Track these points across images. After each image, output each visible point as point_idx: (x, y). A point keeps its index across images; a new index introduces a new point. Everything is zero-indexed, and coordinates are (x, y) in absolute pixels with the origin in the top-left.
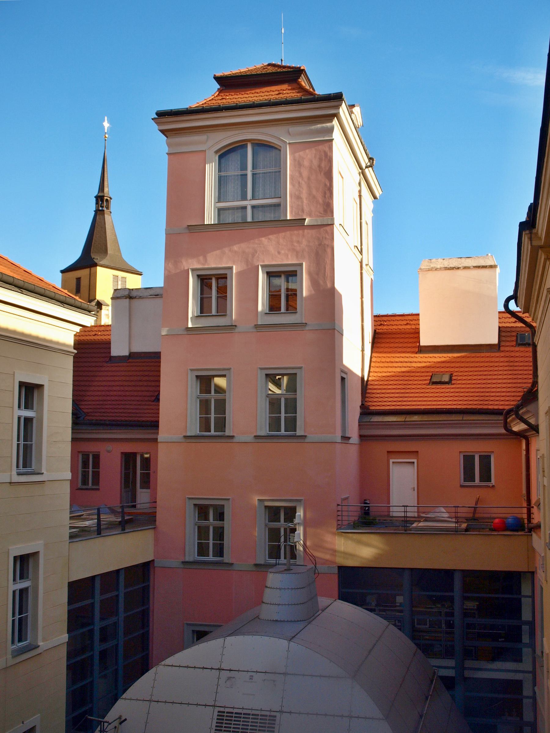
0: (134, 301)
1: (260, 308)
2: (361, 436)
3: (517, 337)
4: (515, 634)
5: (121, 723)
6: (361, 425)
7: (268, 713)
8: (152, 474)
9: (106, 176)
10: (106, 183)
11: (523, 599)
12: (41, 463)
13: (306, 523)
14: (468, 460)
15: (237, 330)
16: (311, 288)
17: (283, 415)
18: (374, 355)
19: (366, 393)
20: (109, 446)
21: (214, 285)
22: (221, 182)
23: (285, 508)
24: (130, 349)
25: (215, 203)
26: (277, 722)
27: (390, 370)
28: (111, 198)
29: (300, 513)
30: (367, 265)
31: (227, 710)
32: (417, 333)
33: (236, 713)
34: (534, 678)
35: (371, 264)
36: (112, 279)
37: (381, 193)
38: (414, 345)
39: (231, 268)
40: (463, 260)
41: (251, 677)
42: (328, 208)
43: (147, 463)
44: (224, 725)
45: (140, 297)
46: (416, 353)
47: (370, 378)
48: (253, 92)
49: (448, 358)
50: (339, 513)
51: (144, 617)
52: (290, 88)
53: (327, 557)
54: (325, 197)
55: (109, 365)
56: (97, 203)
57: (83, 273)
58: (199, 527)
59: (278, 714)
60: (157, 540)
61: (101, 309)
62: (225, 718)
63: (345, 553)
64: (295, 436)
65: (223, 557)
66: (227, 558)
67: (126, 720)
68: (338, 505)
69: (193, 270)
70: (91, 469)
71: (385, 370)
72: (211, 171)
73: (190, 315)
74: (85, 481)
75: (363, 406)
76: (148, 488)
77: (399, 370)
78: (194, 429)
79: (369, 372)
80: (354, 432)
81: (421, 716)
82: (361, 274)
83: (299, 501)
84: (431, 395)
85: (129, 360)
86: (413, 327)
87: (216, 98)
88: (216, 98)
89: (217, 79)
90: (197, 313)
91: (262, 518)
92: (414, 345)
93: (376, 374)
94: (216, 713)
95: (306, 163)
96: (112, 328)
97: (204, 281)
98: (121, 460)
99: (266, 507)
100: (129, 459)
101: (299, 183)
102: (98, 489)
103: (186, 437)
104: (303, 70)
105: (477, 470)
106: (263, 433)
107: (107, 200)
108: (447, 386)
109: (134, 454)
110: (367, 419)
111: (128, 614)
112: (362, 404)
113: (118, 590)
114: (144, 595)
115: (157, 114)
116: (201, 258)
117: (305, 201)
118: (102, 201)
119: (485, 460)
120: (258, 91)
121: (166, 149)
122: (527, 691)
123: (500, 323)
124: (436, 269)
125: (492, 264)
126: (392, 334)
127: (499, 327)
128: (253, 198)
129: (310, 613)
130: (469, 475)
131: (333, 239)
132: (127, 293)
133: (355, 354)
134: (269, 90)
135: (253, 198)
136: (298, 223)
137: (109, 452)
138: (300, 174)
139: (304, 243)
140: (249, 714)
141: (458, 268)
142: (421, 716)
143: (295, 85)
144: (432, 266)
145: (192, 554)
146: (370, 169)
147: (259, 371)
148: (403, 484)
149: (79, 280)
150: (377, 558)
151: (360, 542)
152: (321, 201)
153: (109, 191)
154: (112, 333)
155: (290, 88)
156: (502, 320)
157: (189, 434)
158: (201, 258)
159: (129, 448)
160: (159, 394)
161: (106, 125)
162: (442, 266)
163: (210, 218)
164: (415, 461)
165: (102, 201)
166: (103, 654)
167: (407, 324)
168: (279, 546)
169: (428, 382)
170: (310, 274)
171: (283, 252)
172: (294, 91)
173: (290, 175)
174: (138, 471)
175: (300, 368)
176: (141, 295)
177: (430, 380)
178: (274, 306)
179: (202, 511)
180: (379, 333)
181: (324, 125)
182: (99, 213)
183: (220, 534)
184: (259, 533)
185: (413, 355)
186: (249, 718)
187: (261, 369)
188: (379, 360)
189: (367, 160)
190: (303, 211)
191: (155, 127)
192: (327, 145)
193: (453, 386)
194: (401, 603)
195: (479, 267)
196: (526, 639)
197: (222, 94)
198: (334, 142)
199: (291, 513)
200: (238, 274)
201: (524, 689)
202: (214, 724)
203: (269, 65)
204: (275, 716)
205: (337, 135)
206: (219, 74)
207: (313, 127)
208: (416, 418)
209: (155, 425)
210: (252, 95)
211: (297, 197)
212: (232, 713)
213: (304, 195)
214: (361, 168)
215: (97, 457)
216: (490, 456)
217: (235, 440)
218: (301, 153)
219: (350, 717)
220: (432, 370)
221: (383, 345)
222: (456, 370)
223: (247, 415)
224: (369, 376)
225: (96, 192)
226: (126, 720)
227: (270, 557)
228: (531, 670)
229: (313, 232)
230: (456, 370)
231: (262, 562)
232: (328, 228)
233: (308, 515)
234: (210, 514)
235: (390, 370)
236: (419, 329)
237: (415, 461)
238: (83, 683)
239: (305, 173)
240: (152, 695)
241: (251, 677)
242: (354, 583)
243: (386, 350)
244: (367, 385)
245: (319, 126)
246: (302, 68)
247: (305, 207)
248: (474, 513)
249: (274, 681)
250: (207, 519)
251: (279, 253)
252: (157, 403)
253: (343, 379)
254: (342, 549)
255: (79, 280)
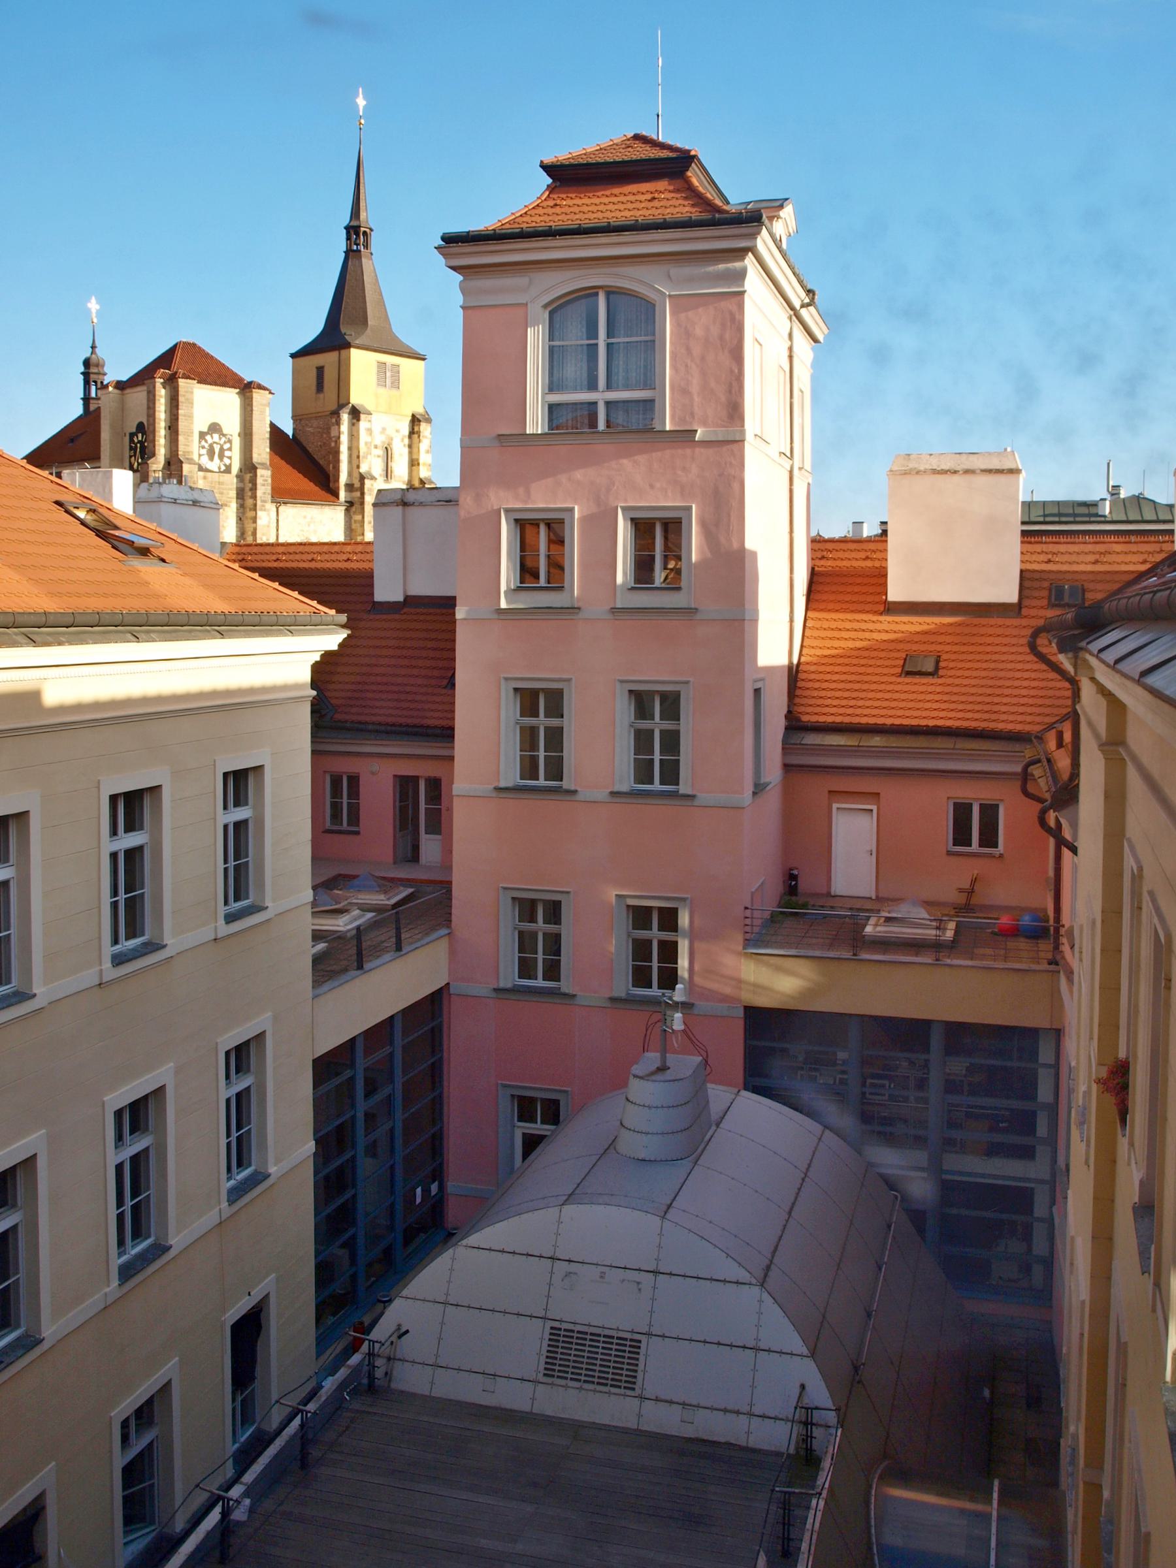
0: (410, 510)
1: (620, 579)
2: (787, 767)
3: (1050, 590)
4: (1026, 1121)
5: (400, 1337)
6: (786, 748)
7: (628, 1336)
8: (443, 811)
9: (362, 191)
10: (362, 204)
11: (1035, 1224)
12: (263, 892)
13: (693, 936)
14: (962, 812)
15: (581, 615)
16: (706, 549)
17: (657, 757)
18: (810, 614)
19: (795, 687)
20: (375, 765)
21: (542, 547)
22: (554, 356)
23: (660, 909)
24: (405, 591)
25: (544, 394)
26: (643, 1351)
27: (836, 644)
28: (371, 230)
29: (684, 920)
30: (800, 469)
31: (564, 1326)
32: (881, 576)
33: (579, 1332)
34: (1053, 1191)
35: (808, 466)
36: (374, 370)
37: (826, 331)
38: (877, 599)
39: (572, 510)
40: (964, 457)
41: (602, 1275)
42: (734, 411)
43: (436, 787)
44: (560, 1350)
45: (421, 504)
46: (881, 614)
47: (803, 659)
48: (608, 192)
49: (933, 626)
50: (748, 921)
51: (436, 1073)
52: (671, 188)
53: (728, 990)
54: (730, 392)
55: (372, 617)
56: (348, 238)
57: (328, 359)
58: (521, 933)
59: (643, 1338)
60: (452, 952)
61: (358, 420)
62: (561, 1339)
63: (755, 985)
64: (674, 795)
65: (559, 980)
66: (565, 985)
67: (407, 1332)
68: (746, 908)
69: (507, 511)
70: (345, 800)
71: (829, 643)
72: (536, 339)
73: (503, 587)
74: (336, 815)
75: (790, 716)
76: (439, 832)
77: (851, 644)
78: (511, 775)
79: (802, 646)
80: (773, 773)
81: (869, 1315)
82: (791, 491)
83: (684, 900)
84: (903, 696)
85: (405, 610)
86: (877, 564)
87: (545, 204)
88: (545, 204)
89: (548, 168)
90: (515, 583)
91: (623, 922)
92: (877, 599)
93: (812, 652)
94: (548, 1330)
95: (699, 331)
96: (375, 548)
97: (524, 526)
98: (394, 786)
99: (628, 906)
100: (406, 786)
101: (687, 366)
102: (358, 833)
103: (498, 789)
104: (695, 157)
105: (972, 827)
106: (624, 788)
107: (365, 233)
108: (930, 680)
109: (415, 779)
110: (797, 738)
111: (411, 1038)
112: (789, 712)
113: (391, 1043)
114: (434, 1039)
115: (443, 239)
116: (521, 490)
117: (696, 399)
118: (358, 235)
119: (990, 813)
120: (616, 191)
121: (459, 299)
122: (1039, 1211)
123: (1022, 562)
124: (918, 473)
125: (1013, 466)
126: (843, 575)
127: (1022, 571)
128: (609, 387)
129: (694, 1133)
130: (961, 836)
131: (743, 466)
132: (398, 496)
133: (777, 635)
134: (635, 191)
135: (609, 387)
136: (684, 436)
137: (373, 773)
138: (689, 350)
139: (695, 470)
140: (599, 1335)
141: (955, 472)
142: (869, 1315)
143: (679, 183)
144: (911, 465)
145: (509, 976)
146: (811, 308)
147: (618, 684)
148: (853, 848)
149: (320, 370)
150: (806, 994)
151: (778, 969)
152: (723, 399)
153: (368, 217)
154: (375, 555)
155: (671, 188)
156: (1026, 558)
157: (502, 784)
158: (521, 490)
159: (408, 769)
160: (454, 674)
161: (361, 102)
162: (928, 467)
163: (535, 422)
164: (874, 808)
165: (355, 233)
166: (370, 1117)
167: (867, 558)
168: (653, 962)
169: (899, 670)
170: (703, 524)
171: (658, 485)
172: (679, 196)
173: (672, 352)
174: (422, 806)
175: (687, 682)
176: (422, 500)
177: (903, 666)
178: (643, 568)
179: (527, 908)
180: (821, 574)
181: (730, 265)
182: (352, 255)
183: (554, 944)
184: (616, 946)
185: (875, 618)
186: (598, 1341)
187: (622, 682)
188: (818, 624)
189: (803, 294)
190: (692, 415)
191: (441, 260)
192: (735, 300)
193: (940, 681)
194: (844, 1061)
195: (990, 471)
196: (1042, 1130)
197: (555, 196)
198: (746, 296)
199: (669, 919)
200: (583, 519)
201: (1041, 1054)
202: (545, 1348)
203: (637, 137)
204: (640, 1341)
205: (754, 284)
206: (549, 159)
207: (711, 269)
208: (876, 741)
209: (447, 734)
210: (606, 200)
211: (682, 390)
212: (573, 1331)
213: (695, 388)
214: (792, 308)
215: (354, 780)
216: (997, 806)
217: (580, 797)
218: (690, 314)
219: (757, 1349)
220: (907, 647)
221: (824, 597)
222: (948, 648)
223: (600, 748)
224: (801, 655)
225: (345, 220)
226: (407, 1332)
227: (639, 780)
228: (1047, 1177)
229: (710, 452)
230: (948, 648)
231: (623, 995)
232: (734, 447)
233: (697, 922)
234: (539, 913)
235: (836, 644)
236: (885, 568)
237: (874, 808)
238: (341, 1201)
239: (697, 350)
240: (447, 1294)
241: (602, 1275)
242: (771, 1045)
243: (831, 606)
244: (797, 671)
245: (721, 267)
246: (693, 153)
247: (696, 409)
248: (969, 899)
249: (638, 1283)
250: (533, 919)
251: (652, 486)
252: (450, 692)
253: (757, 692)
254: (752, 979)
255: (320, 370)
